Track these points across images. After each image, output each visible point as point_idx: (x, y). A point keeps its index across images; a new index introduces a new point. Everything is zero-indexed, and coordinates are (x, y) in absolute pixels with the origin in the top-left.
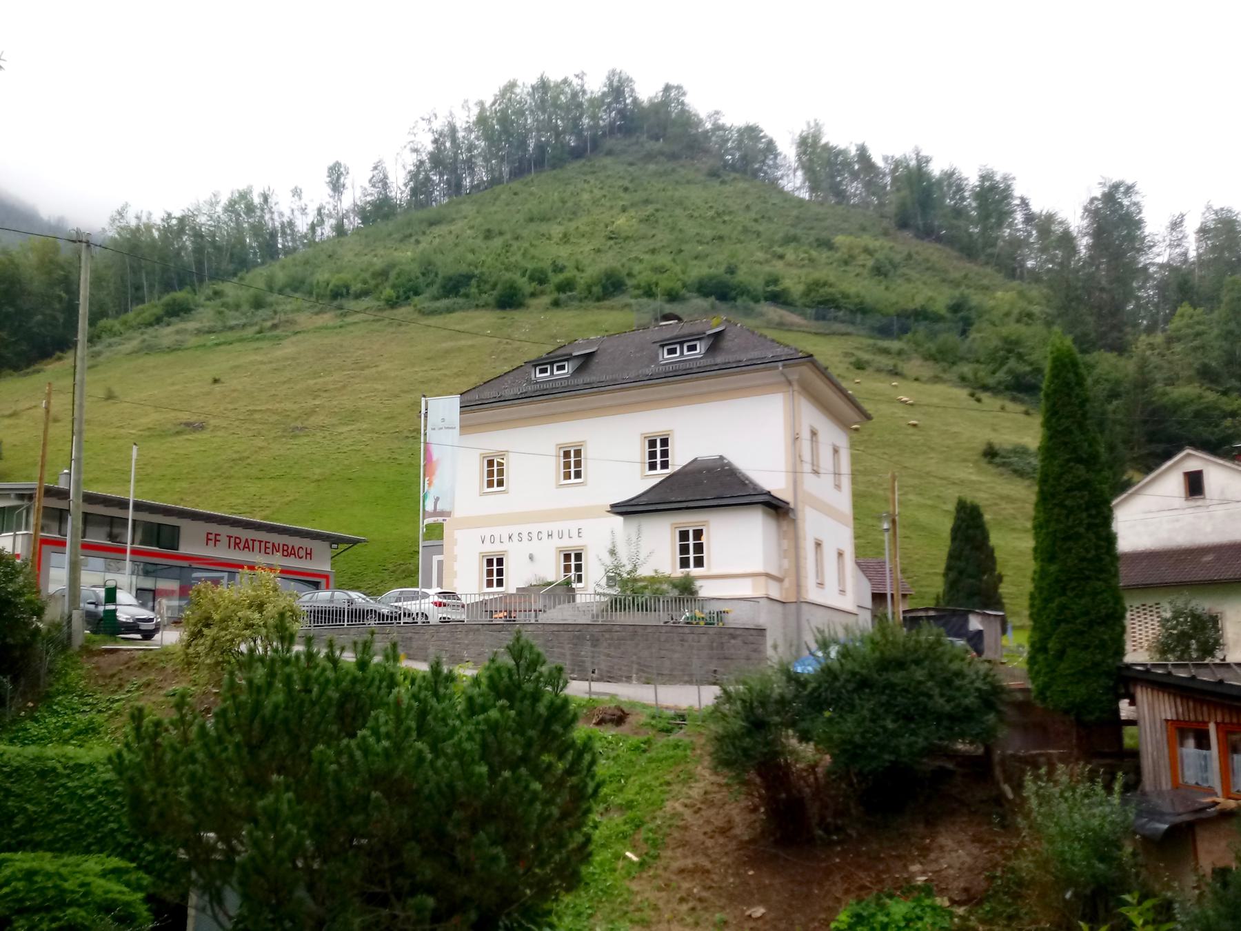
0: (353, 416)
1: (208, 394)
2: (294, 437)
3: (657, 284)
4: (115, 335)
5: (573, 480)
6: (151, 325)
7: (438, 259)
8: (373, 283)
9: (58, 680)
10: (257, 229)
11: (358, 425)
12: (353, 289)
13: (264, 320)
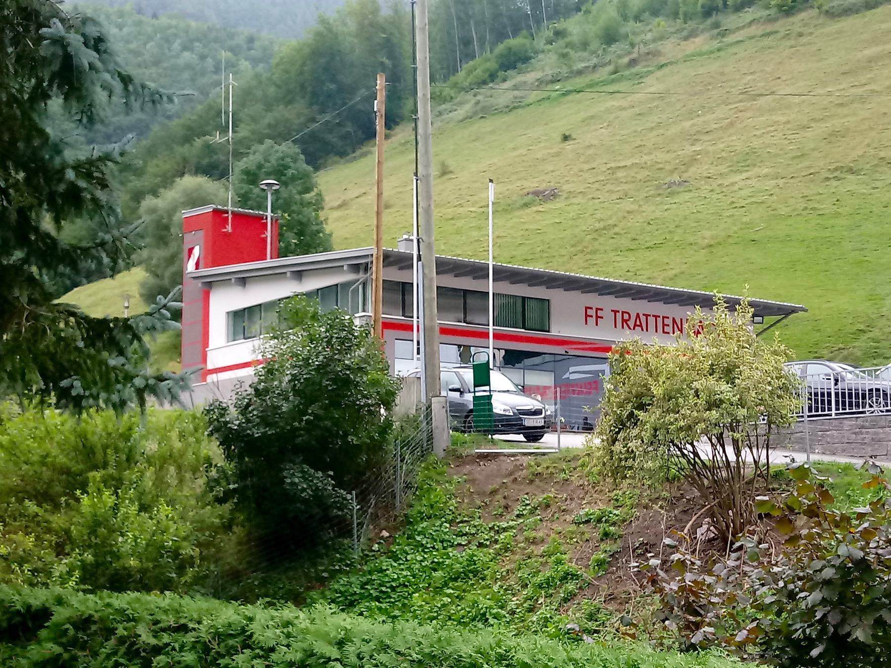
0: (747, 160)
1: (558, 154)
4: (445, 101)
6: (484, 83)
9: (419, 499)
11: (756, 171)
13: (620, 57)
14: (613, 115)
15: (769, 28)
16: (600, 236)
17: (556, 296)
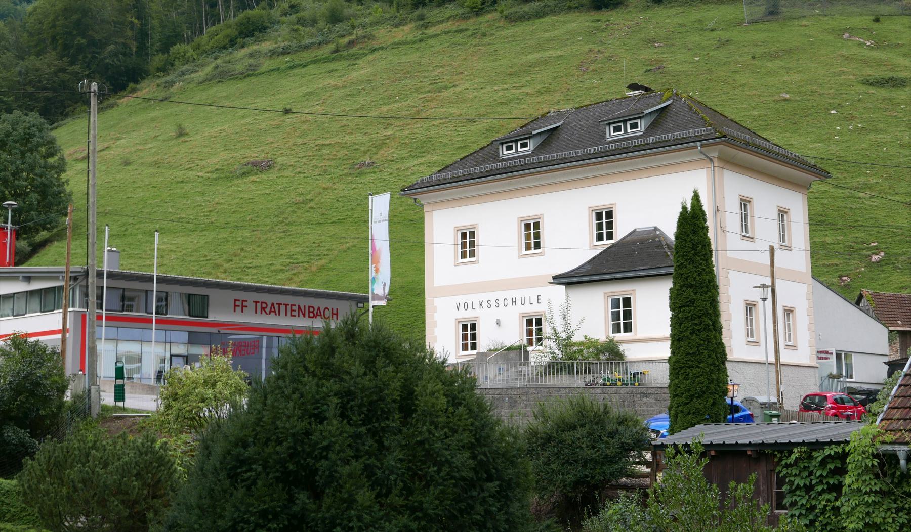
1: (278, 127)
2: (361, 174)
5: (533, 251)
6: (224, 47)
14: (329, 94)
15: (463, 25)
16: (299, 209)
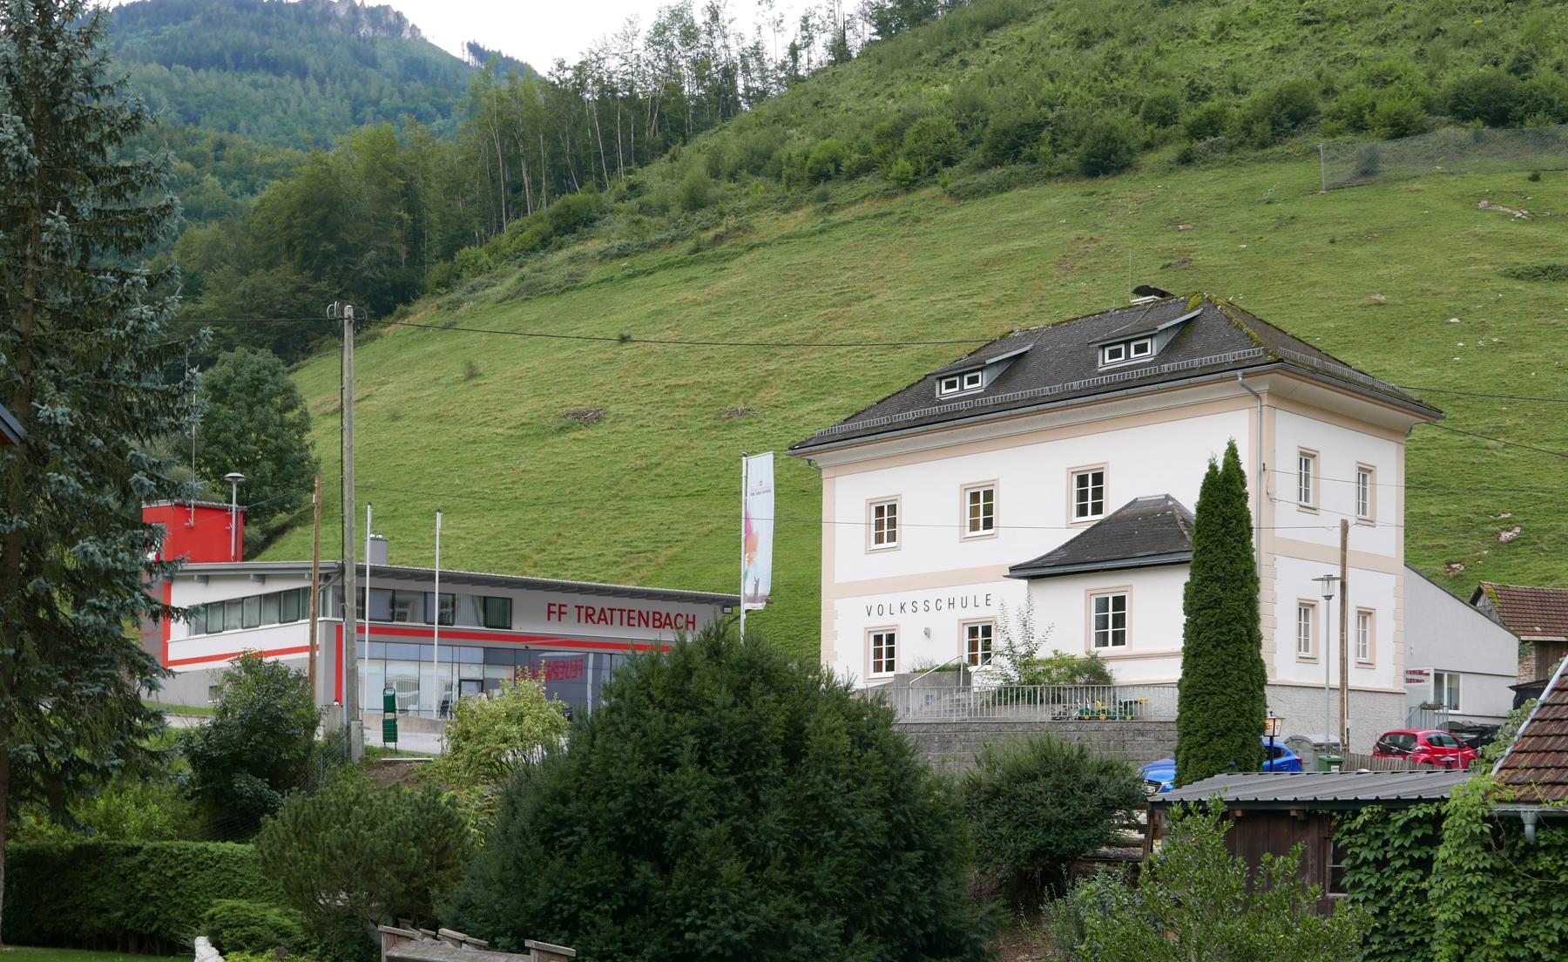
1: (611, 362)
2: (730, 427)
3: (1373, 107)
5: (981, 532)
6: (533, 250)
7: (990, 97)
8: (877, 150)
10: (700, 67)
12: (846, 163)
15: (885, 207)
17: (519, 597)
